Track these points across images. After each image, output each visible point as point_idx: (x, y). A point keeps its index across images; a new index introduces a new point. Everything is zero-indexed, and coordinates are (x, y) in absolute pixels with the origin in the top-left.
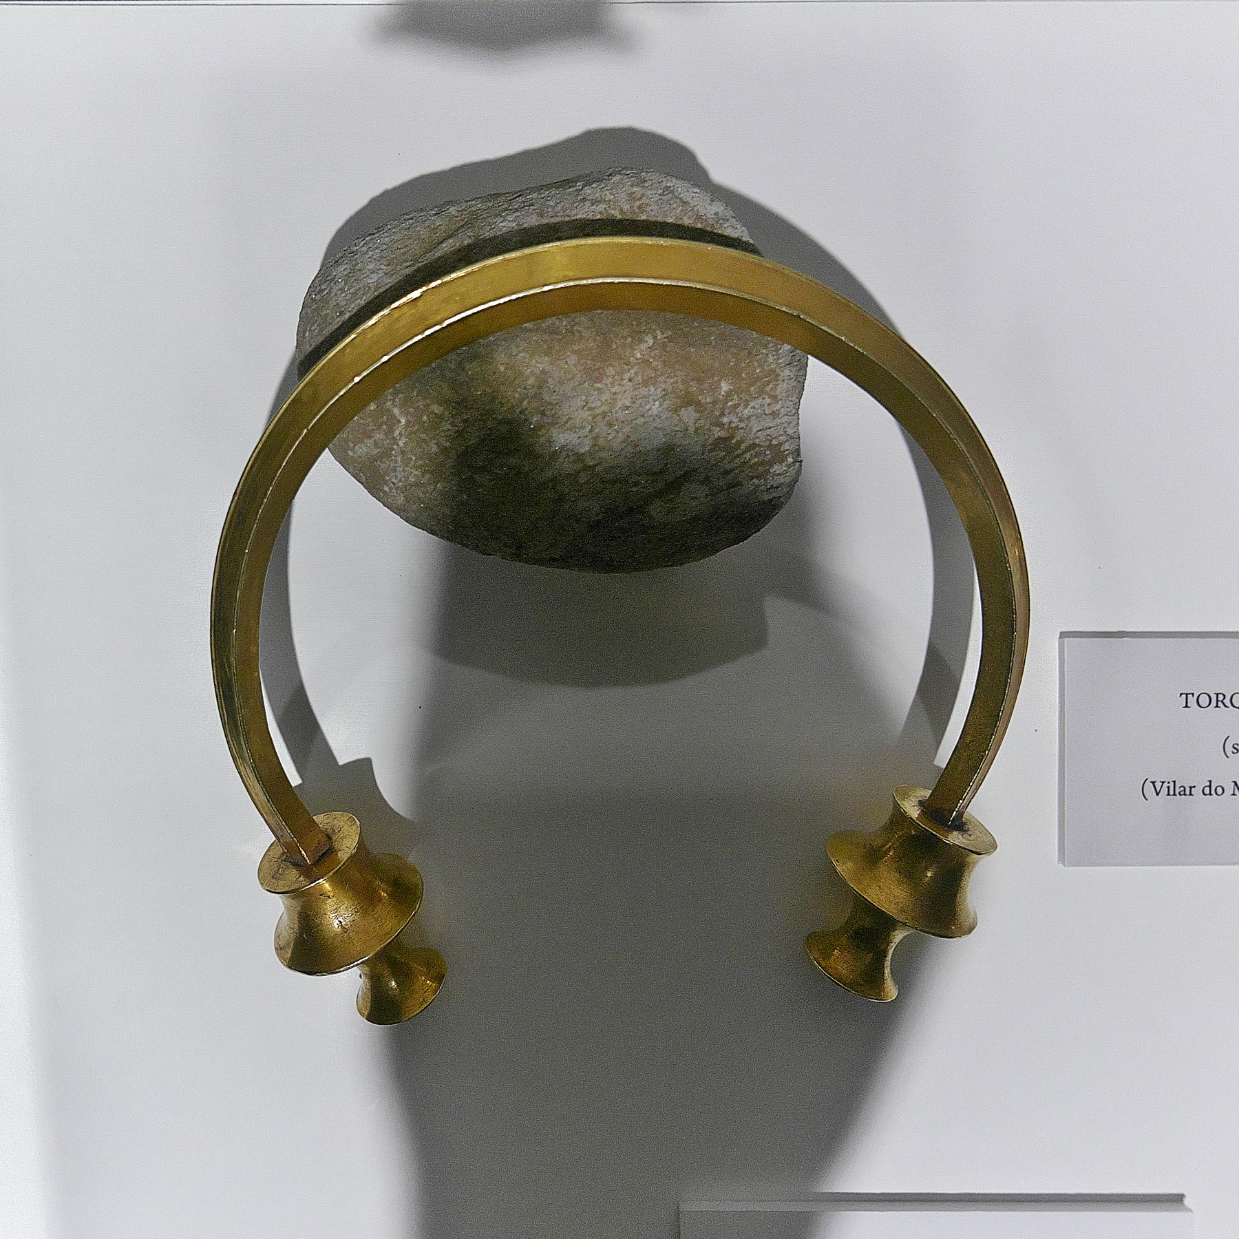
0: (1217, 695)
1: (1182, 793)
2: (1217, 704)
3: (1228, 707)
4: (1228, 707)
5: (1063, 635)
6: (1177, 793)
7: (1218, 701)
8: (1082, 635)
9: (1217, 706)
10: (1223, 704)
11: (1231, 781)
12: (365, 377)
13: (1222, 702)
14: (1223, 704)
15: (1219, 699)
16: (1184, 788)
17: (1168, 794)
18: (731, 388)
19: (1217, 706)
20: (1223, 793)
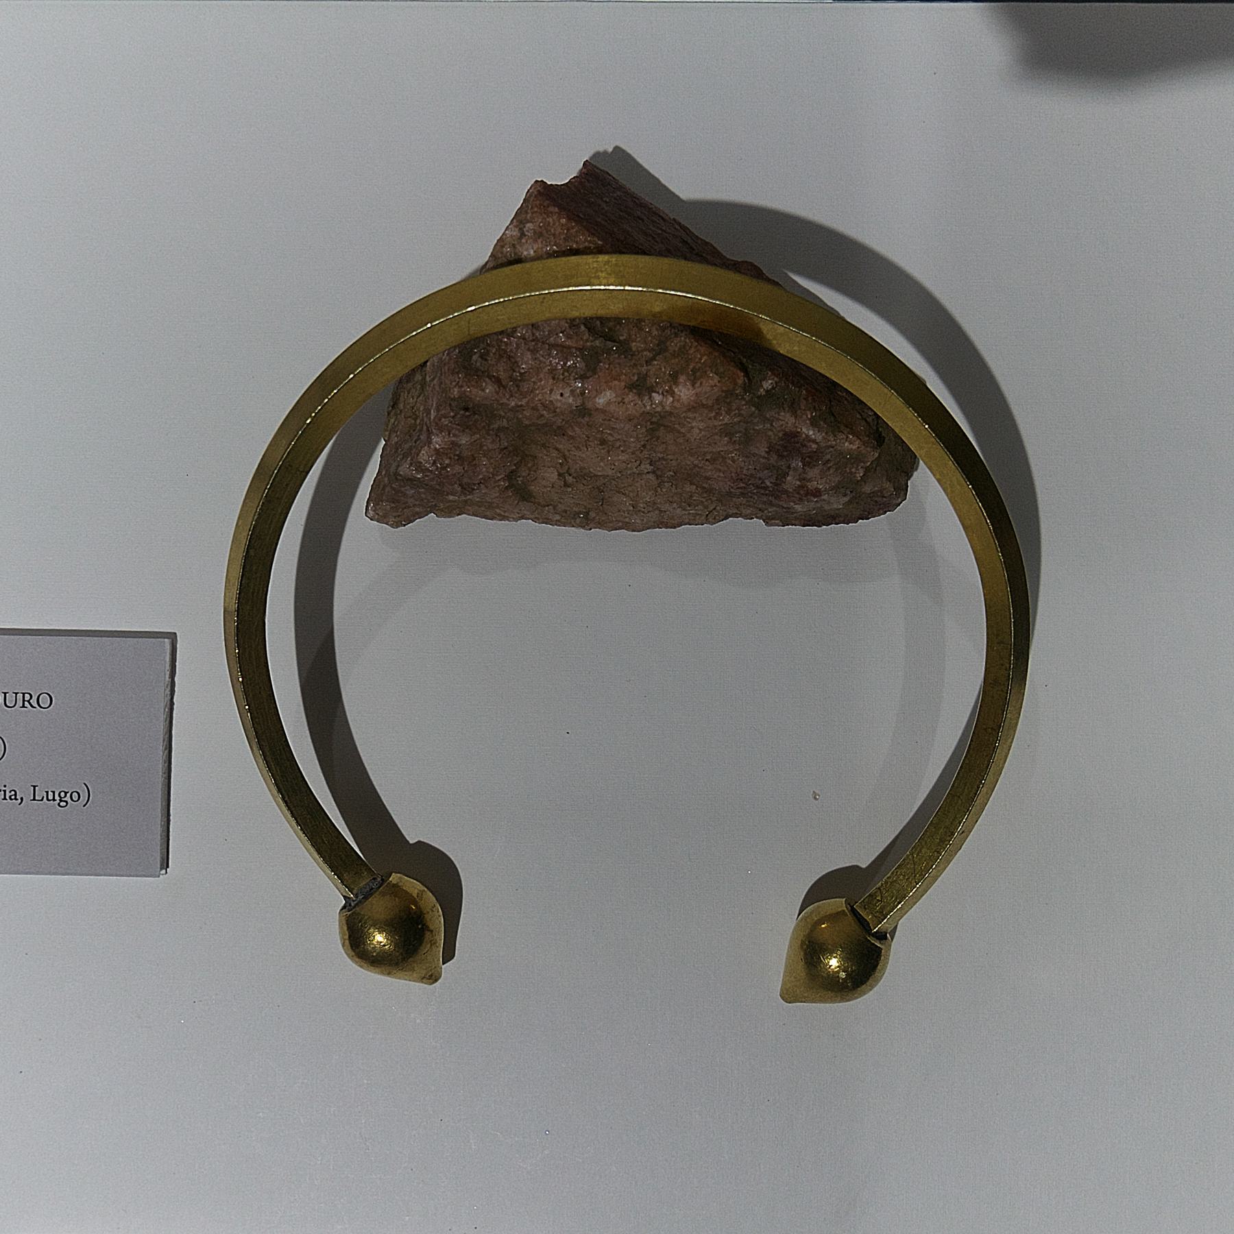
0: (24, 694)
1: (13, 797)
2: (24, 704)
3: (35, 708)
4: (35, 708)
5: (173, 637)
6: (7, 798)
7: (24, 701)
8: (102, 634)
9: (23, 706)
10: (30, 704)
11: (30, 785)
12: (676, 295)
13: (28, 701)
14: (30, 704)
15: (26, 699)
16: (15, 792)
17: (5, 799)
18: (800, 459)
19: (23, 706)
20: (77, 801)
